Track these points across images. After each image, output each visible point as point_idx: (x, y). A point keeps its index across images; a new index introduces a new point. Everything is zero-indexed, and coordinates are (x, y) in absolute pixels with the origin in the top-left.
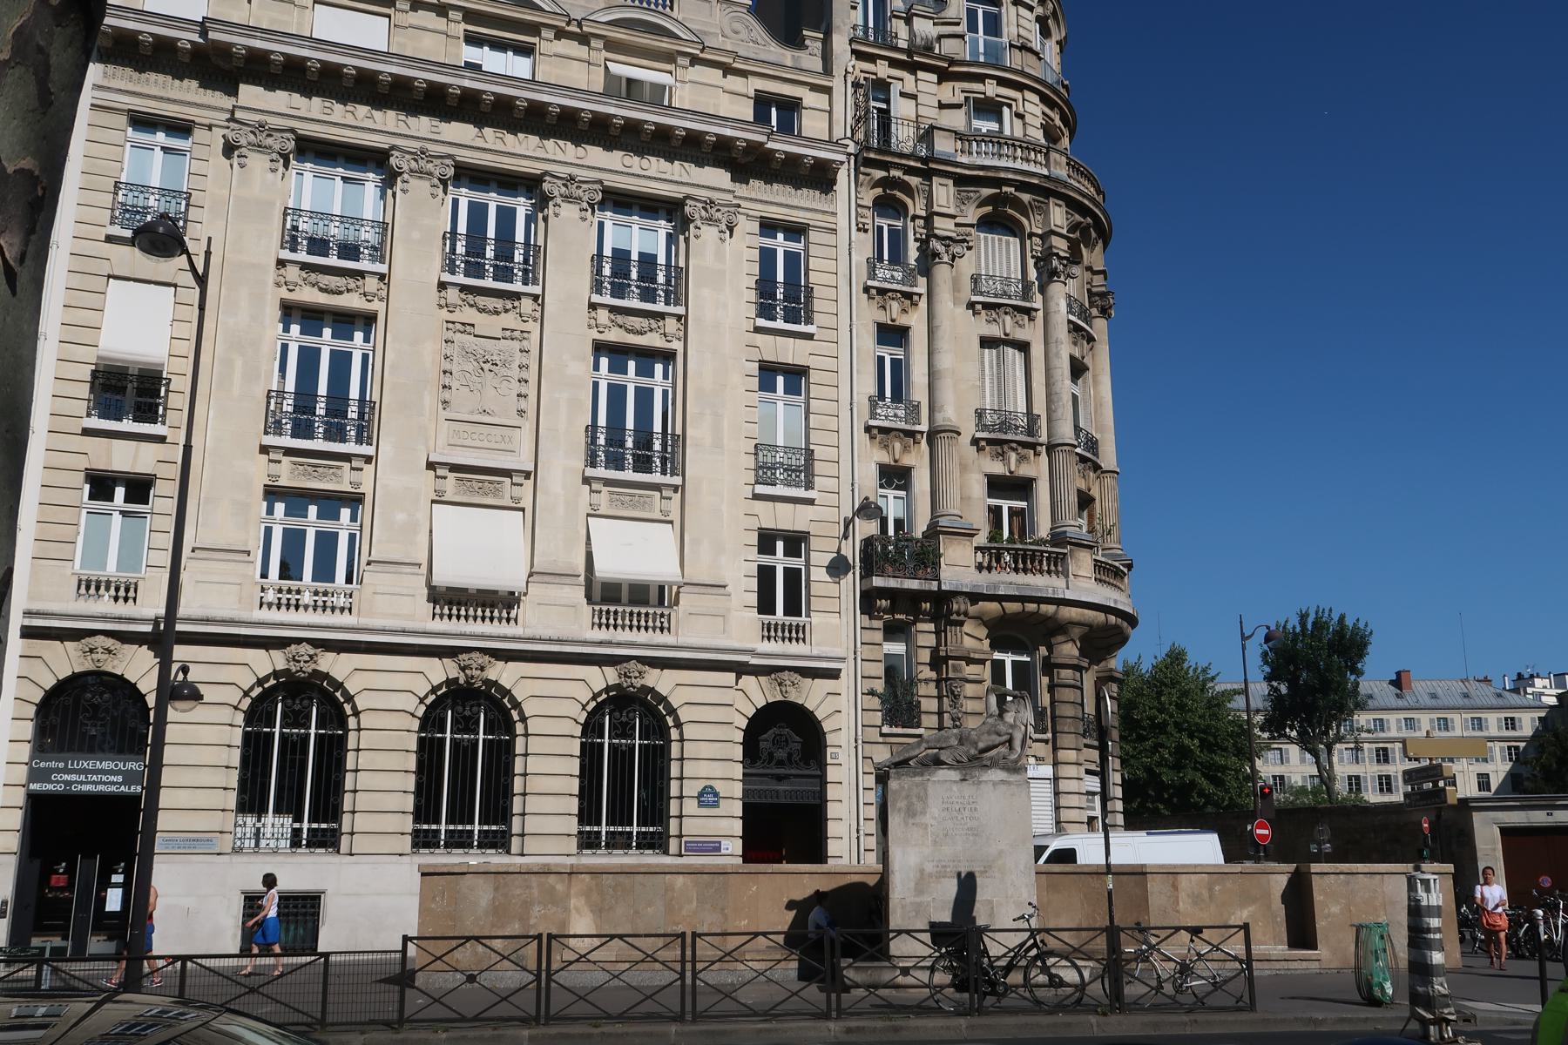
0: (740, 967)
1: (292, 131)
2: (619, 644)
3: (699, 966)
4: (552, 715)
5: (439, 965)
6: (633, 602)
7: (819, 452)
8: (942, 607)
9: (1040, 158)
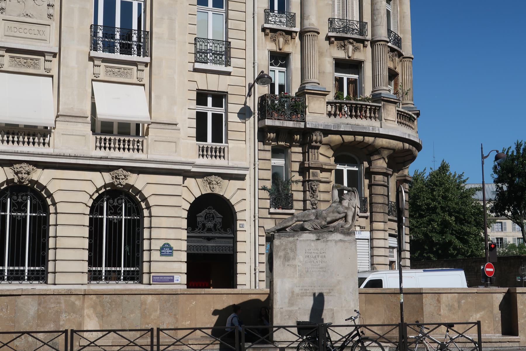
2: (112, 159)
6: (120, 133)
7: (234, 43)
8: (306, 138)
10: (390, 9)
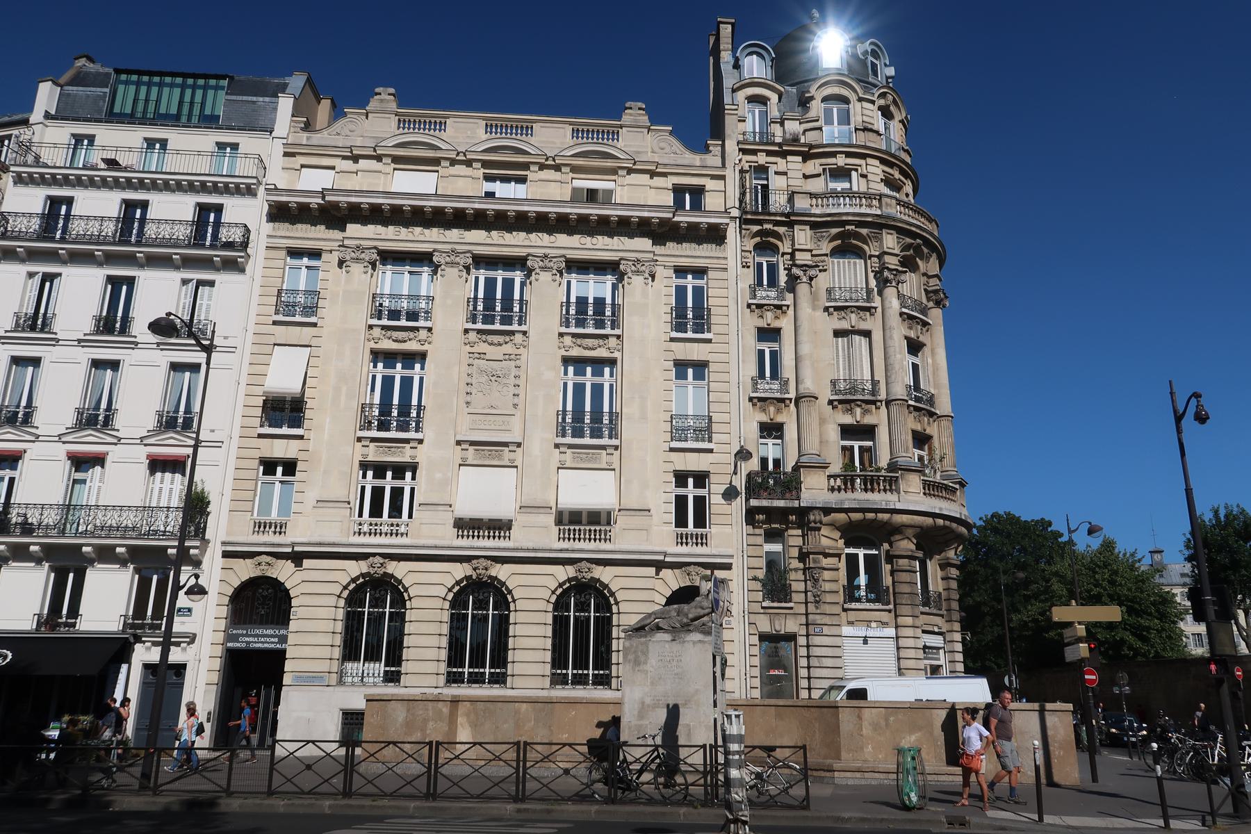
0: (553, 766)
1: (375, 248)
2: (573, 551)
3: (528, 764)
4: (533, 597)
5: (372, 759)
6: (590, 523)
7: (715, 417)
8: (803, 518)
9: (875, 203)
10: (917, 361)
